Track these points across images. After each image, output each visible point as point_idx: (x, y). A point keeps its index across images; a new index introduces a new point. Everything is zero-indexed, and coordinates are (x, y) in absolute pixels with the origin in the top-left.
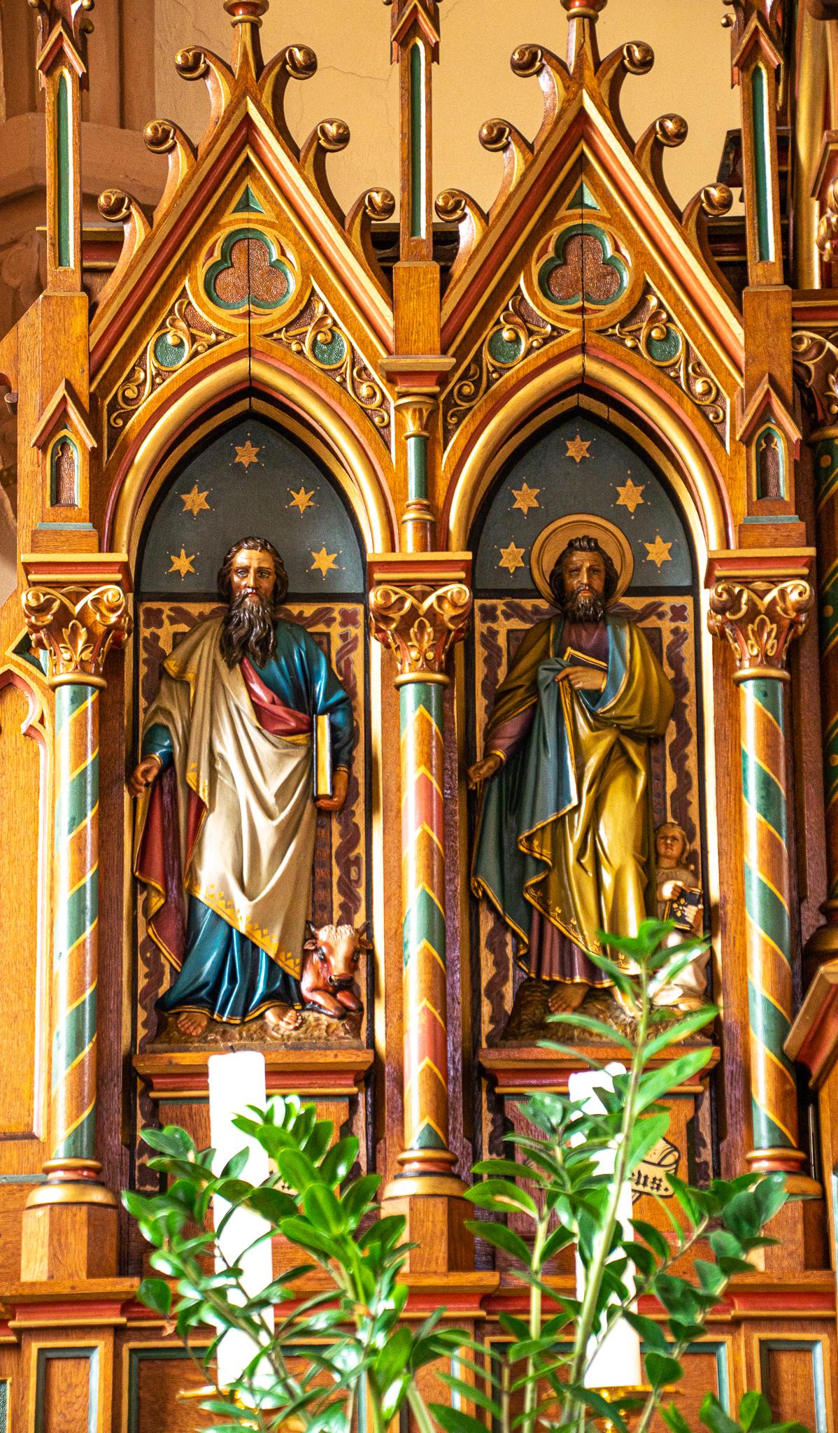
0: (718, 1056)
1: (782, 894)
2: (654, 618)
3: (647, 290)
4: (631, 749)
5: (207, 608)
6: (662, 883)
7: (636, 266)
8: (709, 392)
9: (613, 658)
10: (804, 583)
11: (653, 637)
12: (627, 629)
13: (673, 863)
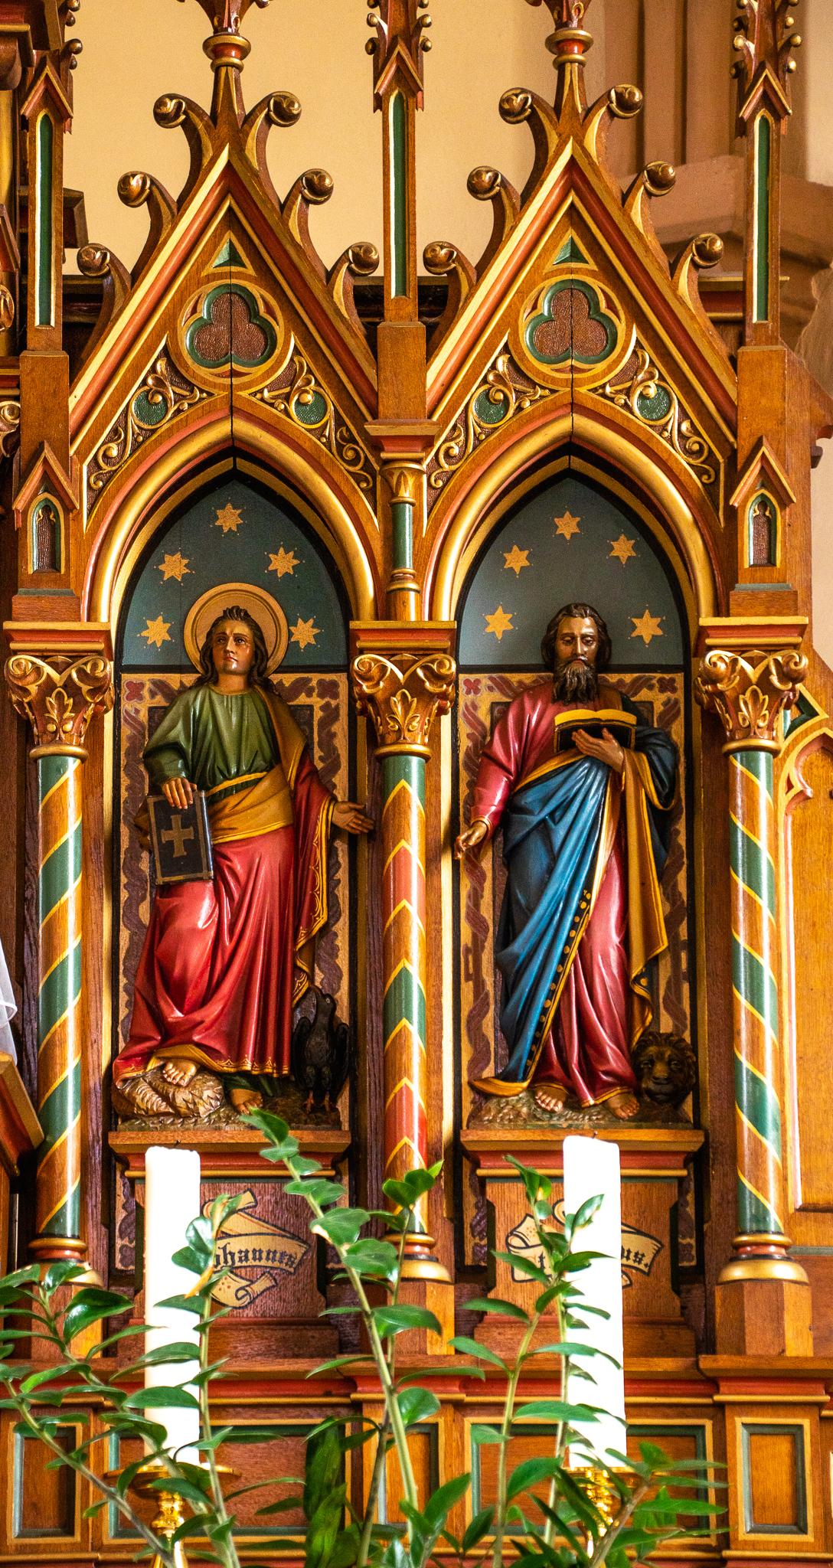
0: (111, 1135)
5: (527, 678)
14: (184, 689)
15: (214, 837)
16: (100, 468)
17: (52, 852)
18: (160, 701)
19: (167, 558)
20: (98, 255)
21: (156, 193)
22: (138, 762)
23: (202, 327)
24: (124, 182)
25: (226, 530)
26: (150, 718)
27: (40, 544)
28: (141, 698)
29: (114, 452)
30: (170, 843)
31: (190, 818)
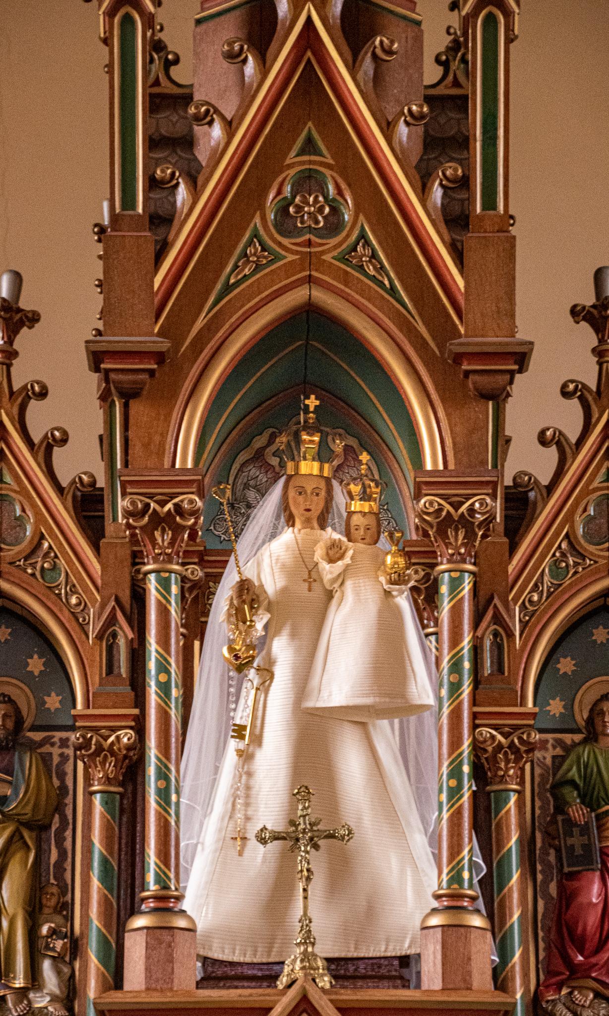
1: (111, 935)
2: (48, 746)
3: (42, 537)
4: (26, 834)
6: (42, 925)
7: (36, 522)
8: (79, 604)
9: (17, 776)
10: (131, 732)
11: (46, 759)
12: (28, 754)
13: (51, 911)
14: (575, 745)
15: (600, 842)
16: (527, 608)
17: (502, 853)
18: (559, 751)
19: (562, 660)
20: (526, 478)
21: (562, 439)
22: (546, 790)
23: (590, 520)
24: (542, 433)
25: (599, 642)
26: (553, 762)
27: (491, 657)
28: (546, 749)
29: (536, 598)
30: (573, 846)
31: (585, 830)
